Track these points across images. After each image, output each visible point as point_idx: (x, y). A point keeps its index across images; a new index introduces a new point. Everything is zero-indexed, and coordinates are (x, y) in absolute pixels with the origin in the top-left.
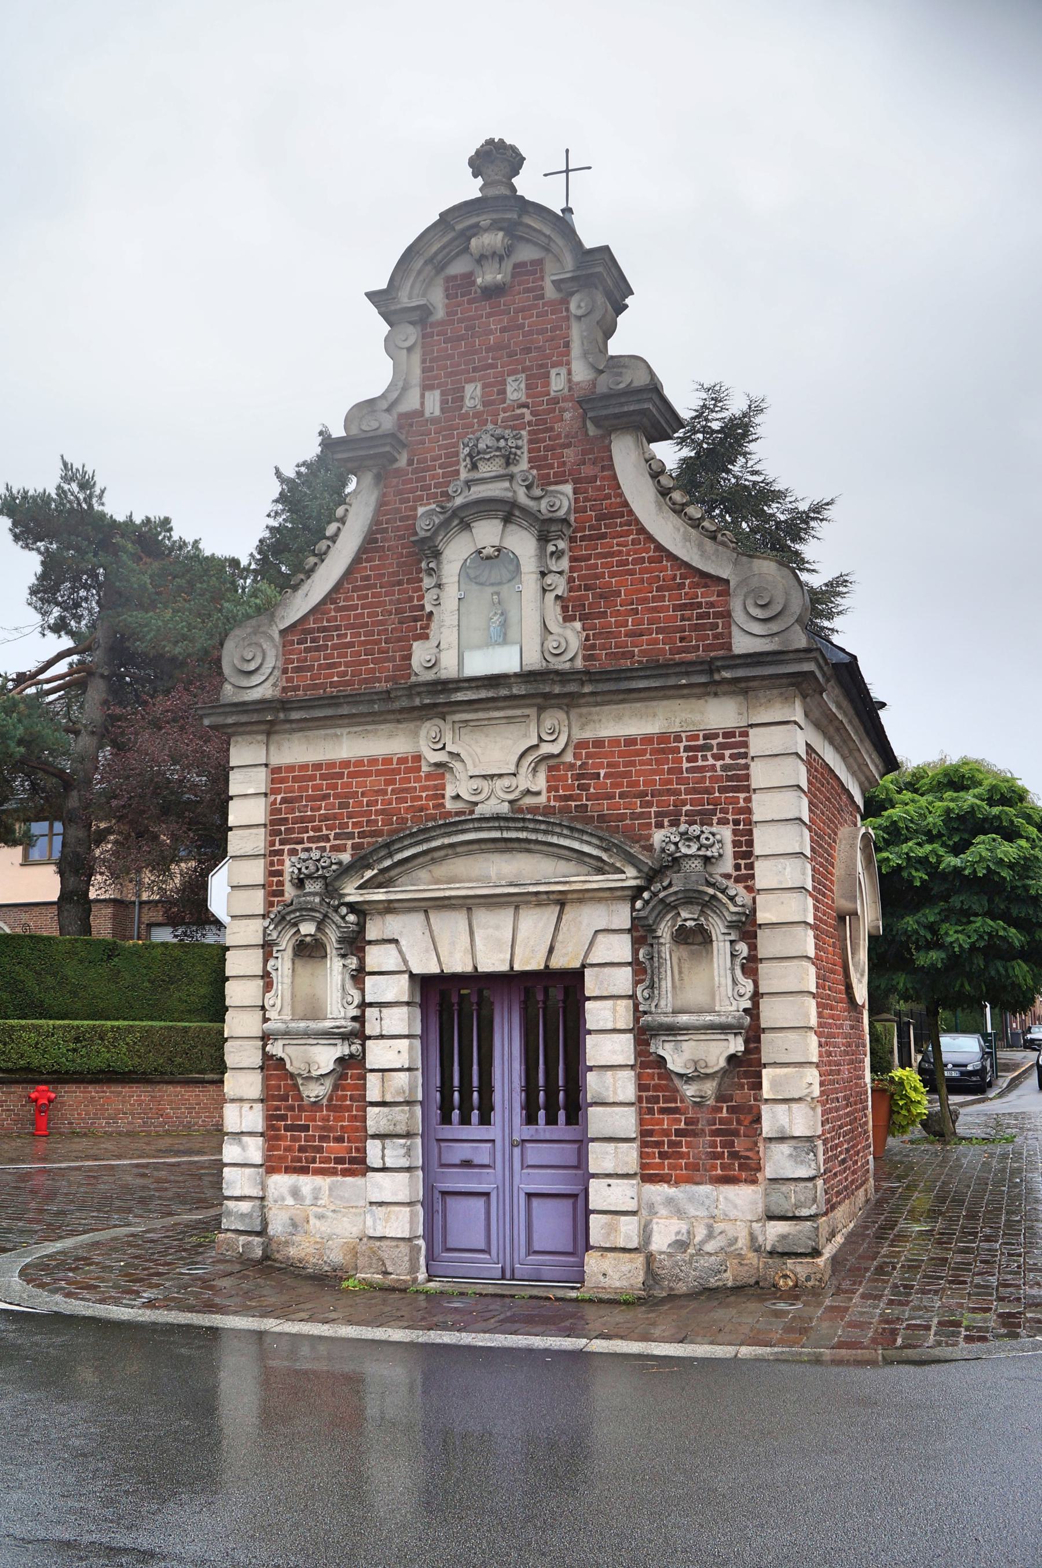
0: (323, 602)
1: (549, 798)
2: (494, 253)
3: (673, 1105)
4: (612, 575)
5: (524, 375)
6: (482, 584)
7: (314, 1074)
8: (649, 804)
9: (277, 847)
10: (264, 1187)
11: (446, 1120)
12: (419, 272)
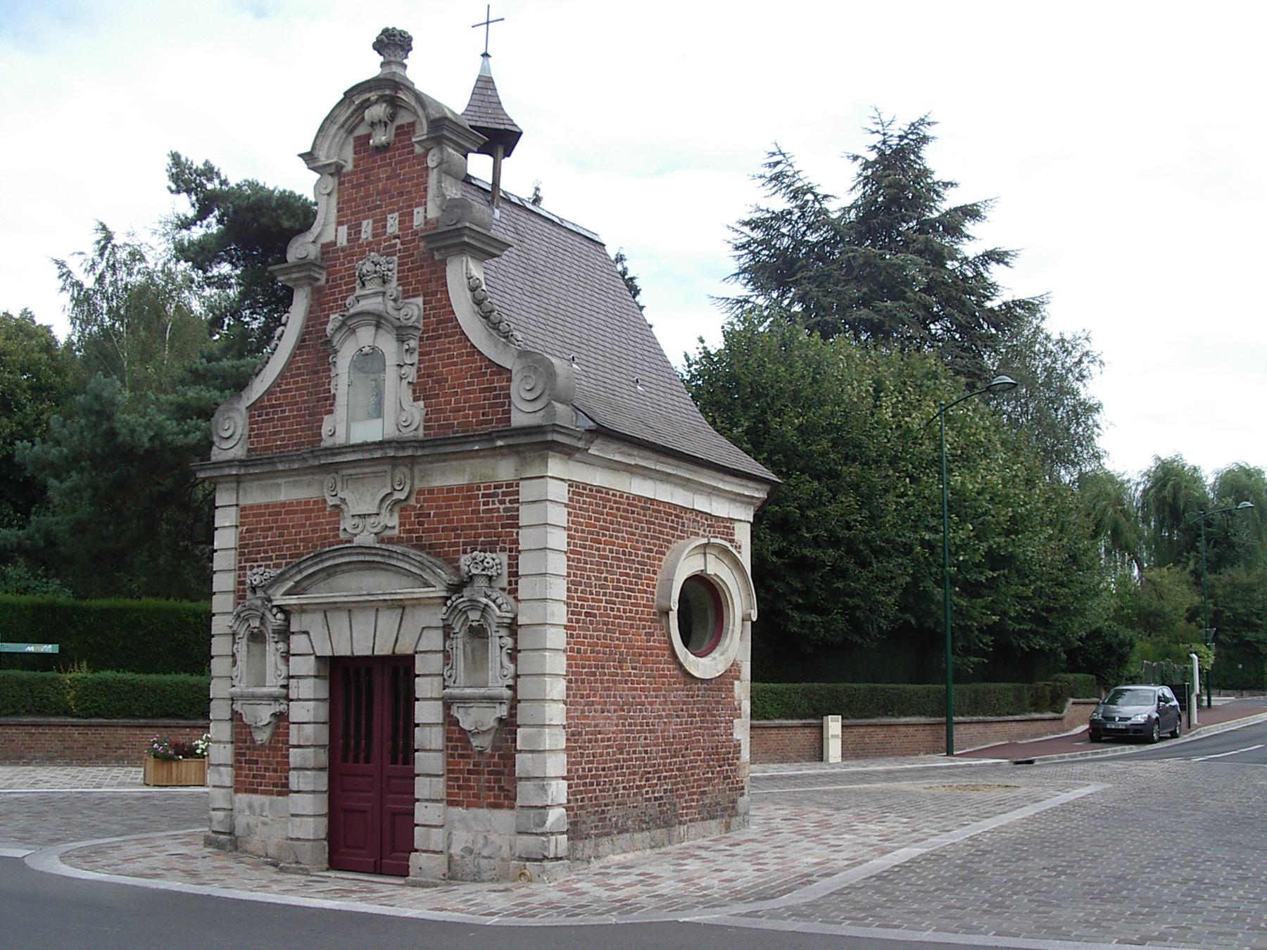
2: (380, 121)
4: (444, 366)
6: (369, 373)
9: (243, 564)
10: (232, 802)
11: (345, 759)
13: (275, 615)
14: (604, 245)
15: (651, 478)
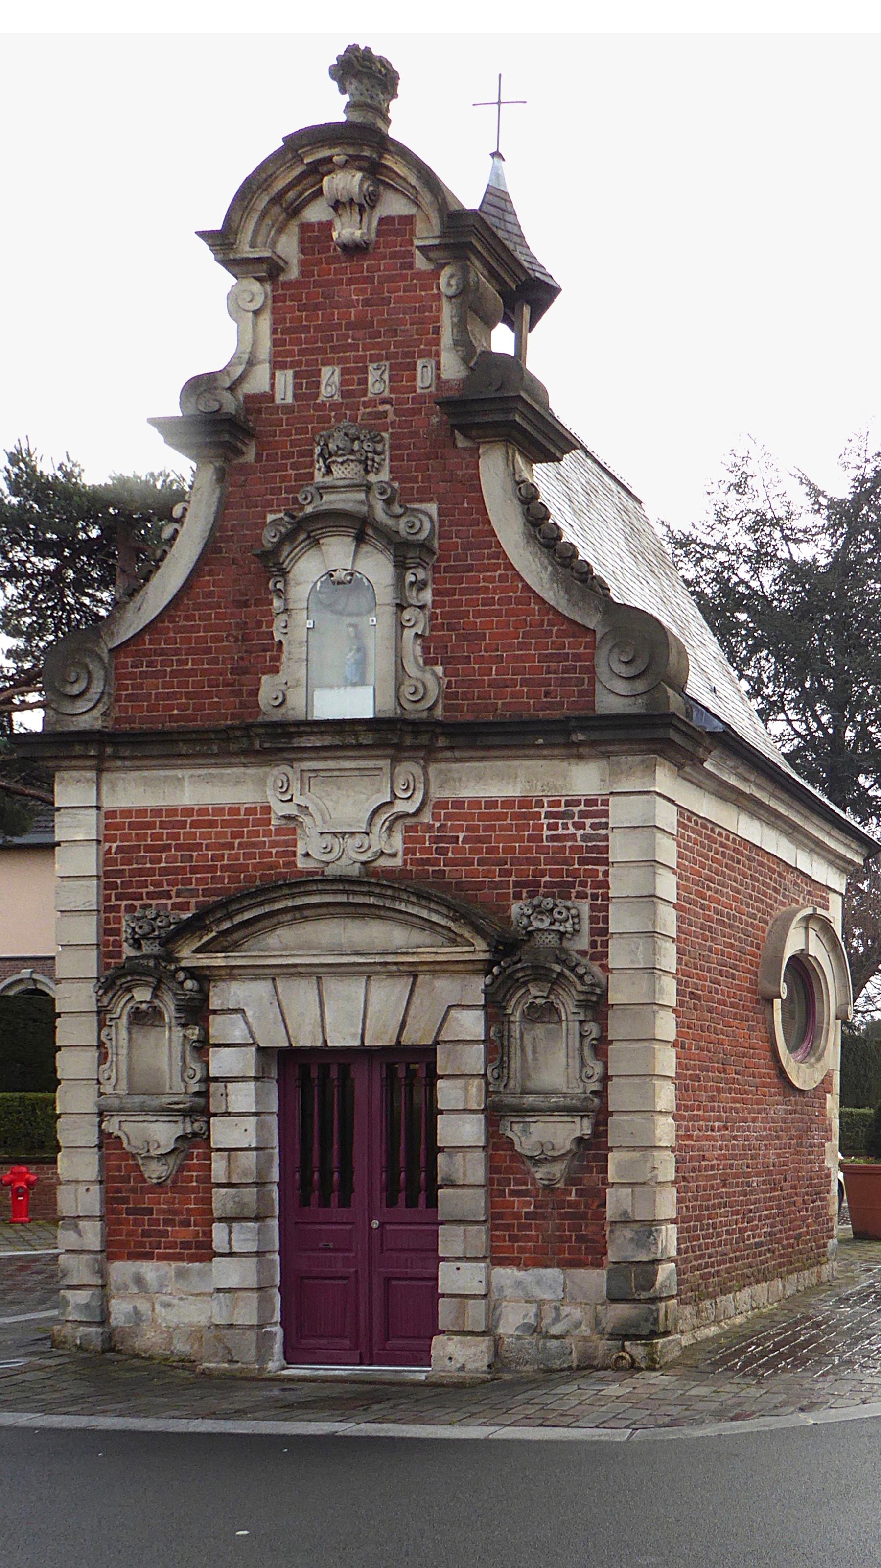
0: (160, 617)
1: (405, 861)
3: (524, 1188)
5: (387, 363)
6: (341, 613)
7: (153, 1153)
8: (508, 873)
10: (102, 1273)
12: (264, 214)
13: (182, 983)
14: (640, 503)
15: (759, 819)
